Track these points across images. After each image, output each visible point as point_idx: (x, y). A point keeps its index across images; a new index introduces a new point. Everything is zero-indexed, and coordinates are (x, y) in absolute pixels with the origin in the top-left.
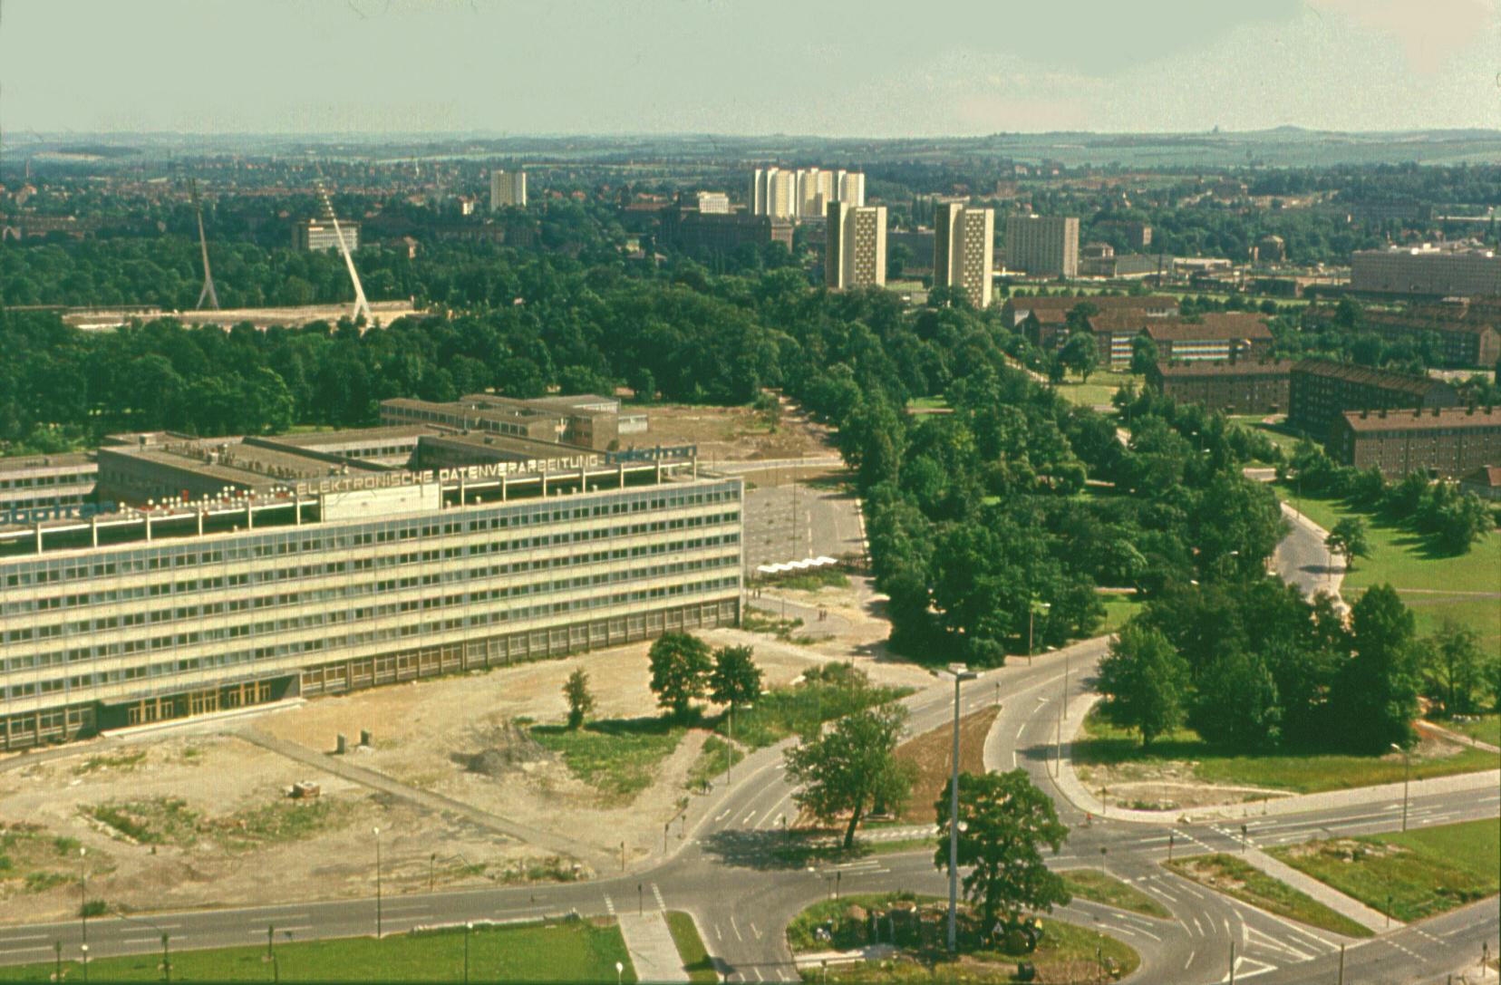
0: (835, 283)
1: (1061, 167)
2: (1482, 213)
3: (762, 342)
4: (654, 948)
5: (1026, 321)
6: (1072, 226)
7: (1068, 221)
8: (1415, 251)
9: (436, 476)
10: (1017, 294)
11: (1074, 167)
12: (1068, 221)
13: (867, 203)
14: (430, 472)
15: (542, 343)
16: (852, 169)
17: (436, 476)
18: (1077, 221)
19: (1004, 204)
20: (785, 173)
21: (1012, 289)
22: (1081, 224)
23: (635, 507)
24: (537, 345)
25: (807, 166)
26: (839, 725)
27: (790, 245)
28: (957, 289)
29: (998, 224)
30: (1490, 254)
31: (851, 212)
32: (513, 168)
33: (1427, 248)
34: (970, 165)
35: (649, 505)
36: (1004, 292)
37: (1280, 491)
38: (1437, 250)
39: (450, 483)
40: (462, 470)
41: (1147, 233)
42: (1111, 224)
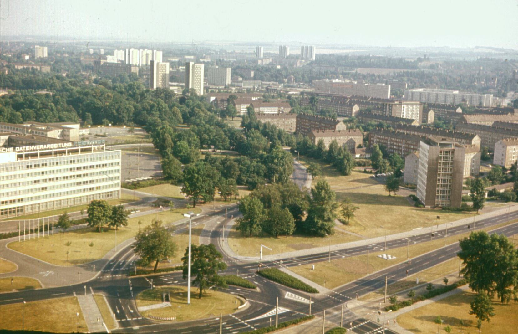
0: (152, 87)
1: (225, 51)
2: (353, 70)
3: (128, 106)
4: (89, 307)
5: (214, 101)
6: (229, 71)
7: (286, 297)
8: (334, 81)
9: (14, 149)
10: (211, 92)
11: (230, 52)
12: (286, 297)
13: (163, 61)
14: (12, 148)
15: (53, 104)
16: (158, 50)
17: (14, 149)
18: (230, 69)
19: (208, 63)
20: (137, 50)
21: (210, 90)
22: (232, 70)
23: (71, 162)
24: (51, 106)
25: (143, 48)
26: (279, 111)
27: (138, 74)
28: (193, 90)
29: (206, 70)
30: (356, 83)
31: (158, 64)
32: (42, 45)
33: (337, 80)
34: (197, 50)
35: (33, 166)
36: (207, 91)
37: (424, 203)
38: (340, 81)
39: (19, 152)
40: (24, 147)
41: (252, 74)
42: (239, 71)
